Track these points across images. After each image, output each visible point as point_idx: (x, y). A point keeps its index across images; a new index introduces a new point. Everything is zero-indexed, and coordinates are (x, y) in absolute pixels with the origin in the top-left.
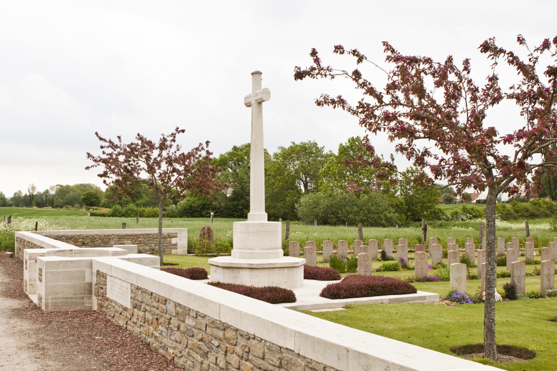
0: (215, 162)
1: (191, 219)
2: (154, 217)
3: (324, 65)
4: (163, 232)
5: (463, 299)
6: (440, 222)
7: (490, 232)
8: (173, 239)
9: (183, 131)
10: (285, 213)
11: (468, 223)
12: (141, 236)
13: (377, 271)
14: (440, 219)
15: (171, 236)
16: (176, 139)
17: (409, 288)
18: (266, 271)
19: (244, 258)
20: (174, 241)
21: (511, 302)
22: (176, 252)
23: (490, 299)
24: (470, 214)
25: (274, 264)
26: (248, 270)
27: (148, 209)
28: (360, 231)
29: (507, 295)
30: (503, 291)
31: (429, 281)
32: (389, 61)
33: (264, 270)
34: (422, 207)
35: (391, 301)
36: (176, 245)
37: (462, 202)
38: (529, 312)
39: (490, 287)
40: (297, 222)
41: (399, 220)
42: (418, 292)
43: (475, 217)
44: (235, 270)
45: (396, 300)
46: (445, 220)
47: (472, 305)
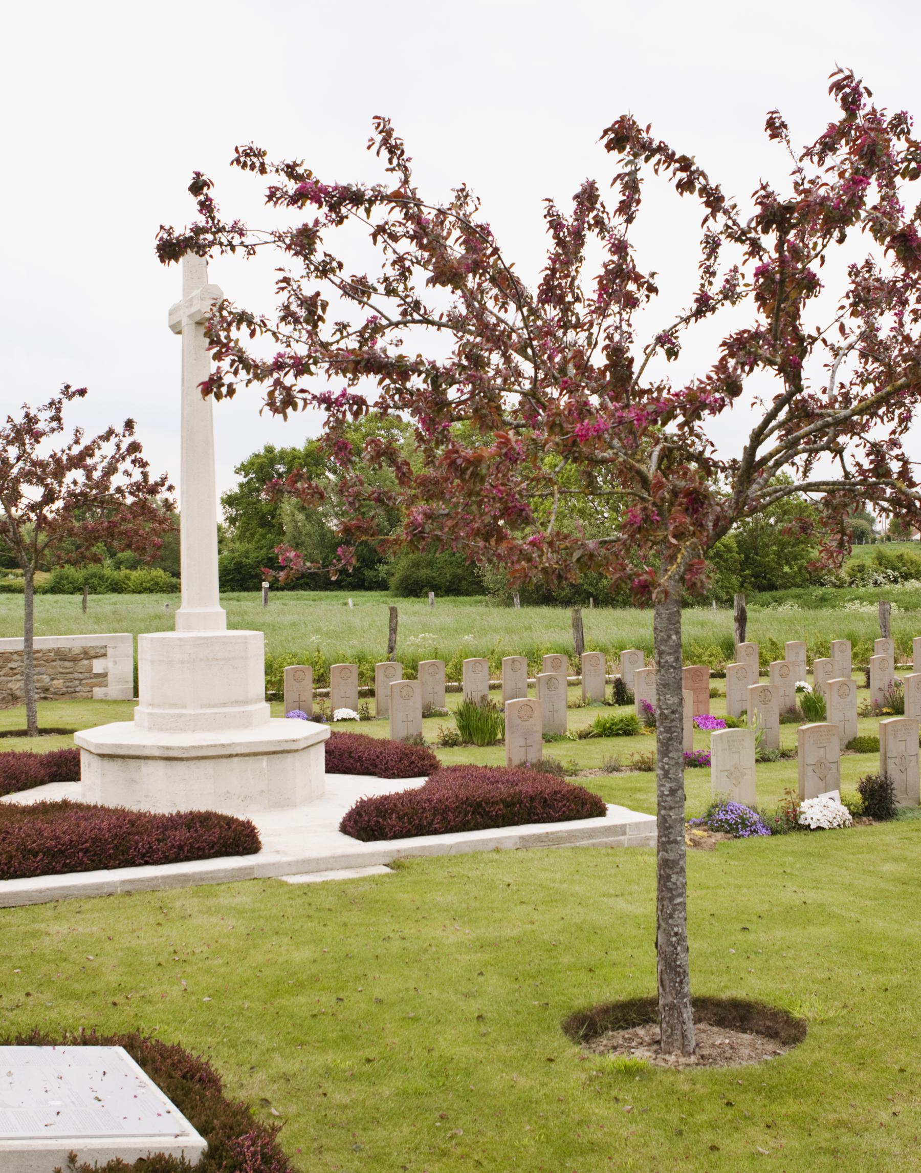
0: (294, 458)
1: (236, 594)
2: (151, 591)
3: (225, 217)
4: (36, 646)
5: (743, 823)
6: (820, 591)
7: (664, 686)
8: (95, 662)
9: (82, 392)
10: (455, 576)
11: (887, 593)
12: (15, 657)
13: (580, 737)
14: (822, 585)
15: (92, 653)
16: (62, 415)
17: (583, 804)
18: (209, 764)
19: (161, 729)
20: (98, 666)
21: (878, 826)
22: (106, 694)
23: (669, 877)
24: (894, 569)
25: (229, 745)
26: (162, 763)
27: (136, 575)
28: (578, 625)
29: (867, 808)
30: (857, 798)
31: (695, 766)
32: (276, 203)
33: (202, 762)
34: (778, 554)
35: (526, 843)
36: (104, 675)
37: (889, 539)
38: (905, 859)
39: (669, 842)
40: (479, 598)
41: (722, 587)
42: (611, 808)
43: (906, 577)
44: (132, 763)
45: (539, 838)
46: (835, 585)
47: (764, 840)
